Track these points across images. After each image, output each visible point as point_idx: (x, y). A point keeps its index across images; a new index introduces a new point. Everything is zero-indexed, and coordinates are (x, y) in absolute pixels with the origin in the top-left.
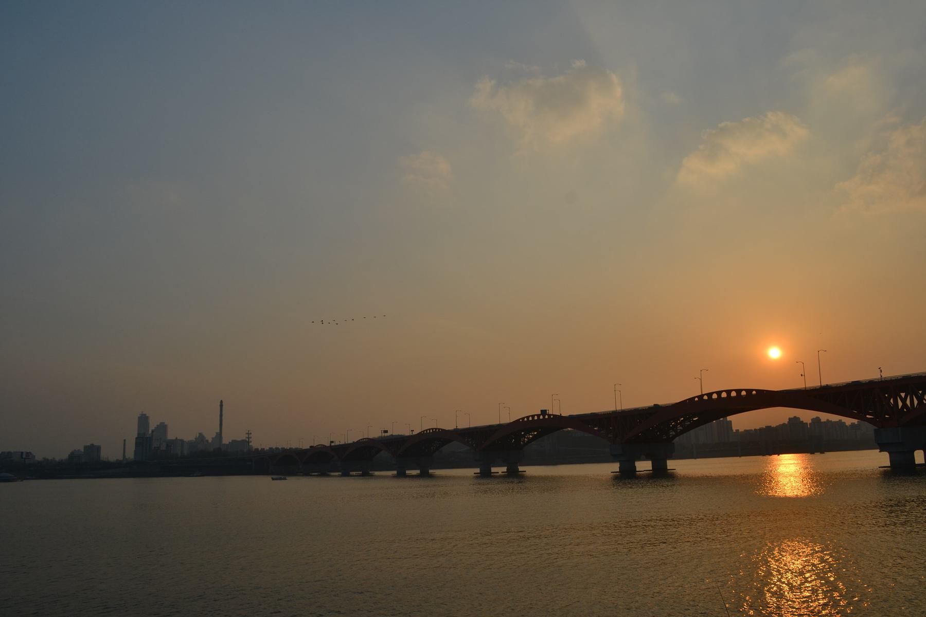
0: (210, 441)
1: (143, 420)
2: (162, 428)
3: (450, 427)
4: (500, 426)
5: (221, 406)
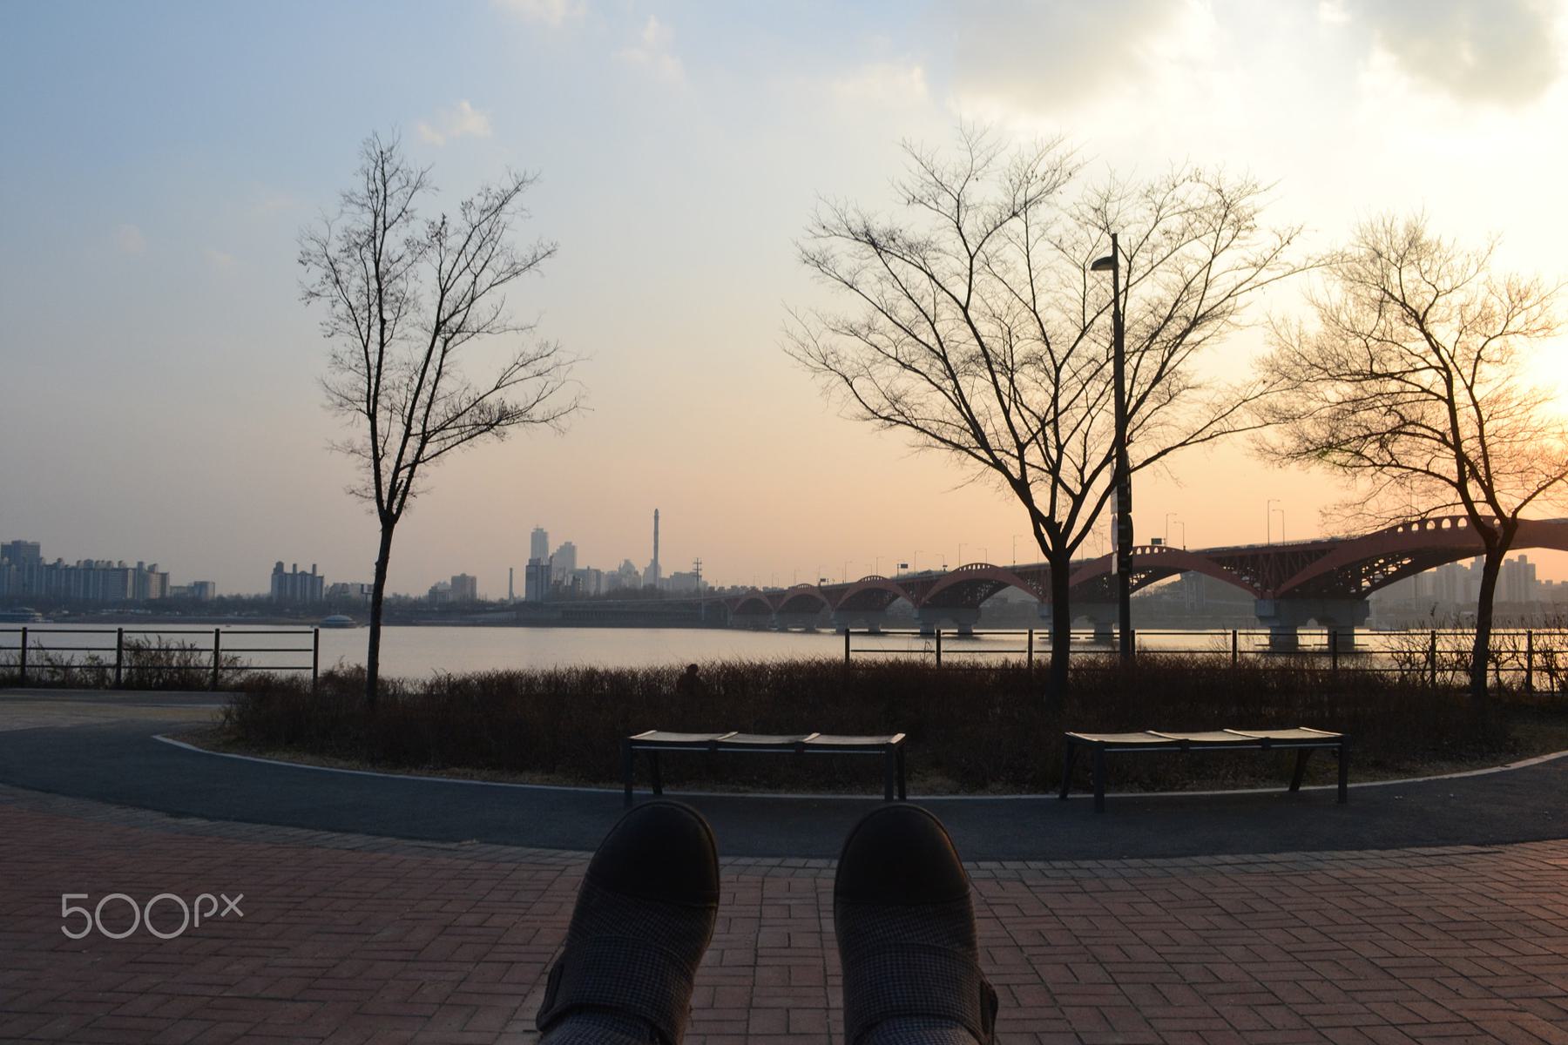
0: (641, 573)
1: (539, 538)
2: (568, 550)
3: (889, 572)
4: (943, 575)
5: (656, 518)
